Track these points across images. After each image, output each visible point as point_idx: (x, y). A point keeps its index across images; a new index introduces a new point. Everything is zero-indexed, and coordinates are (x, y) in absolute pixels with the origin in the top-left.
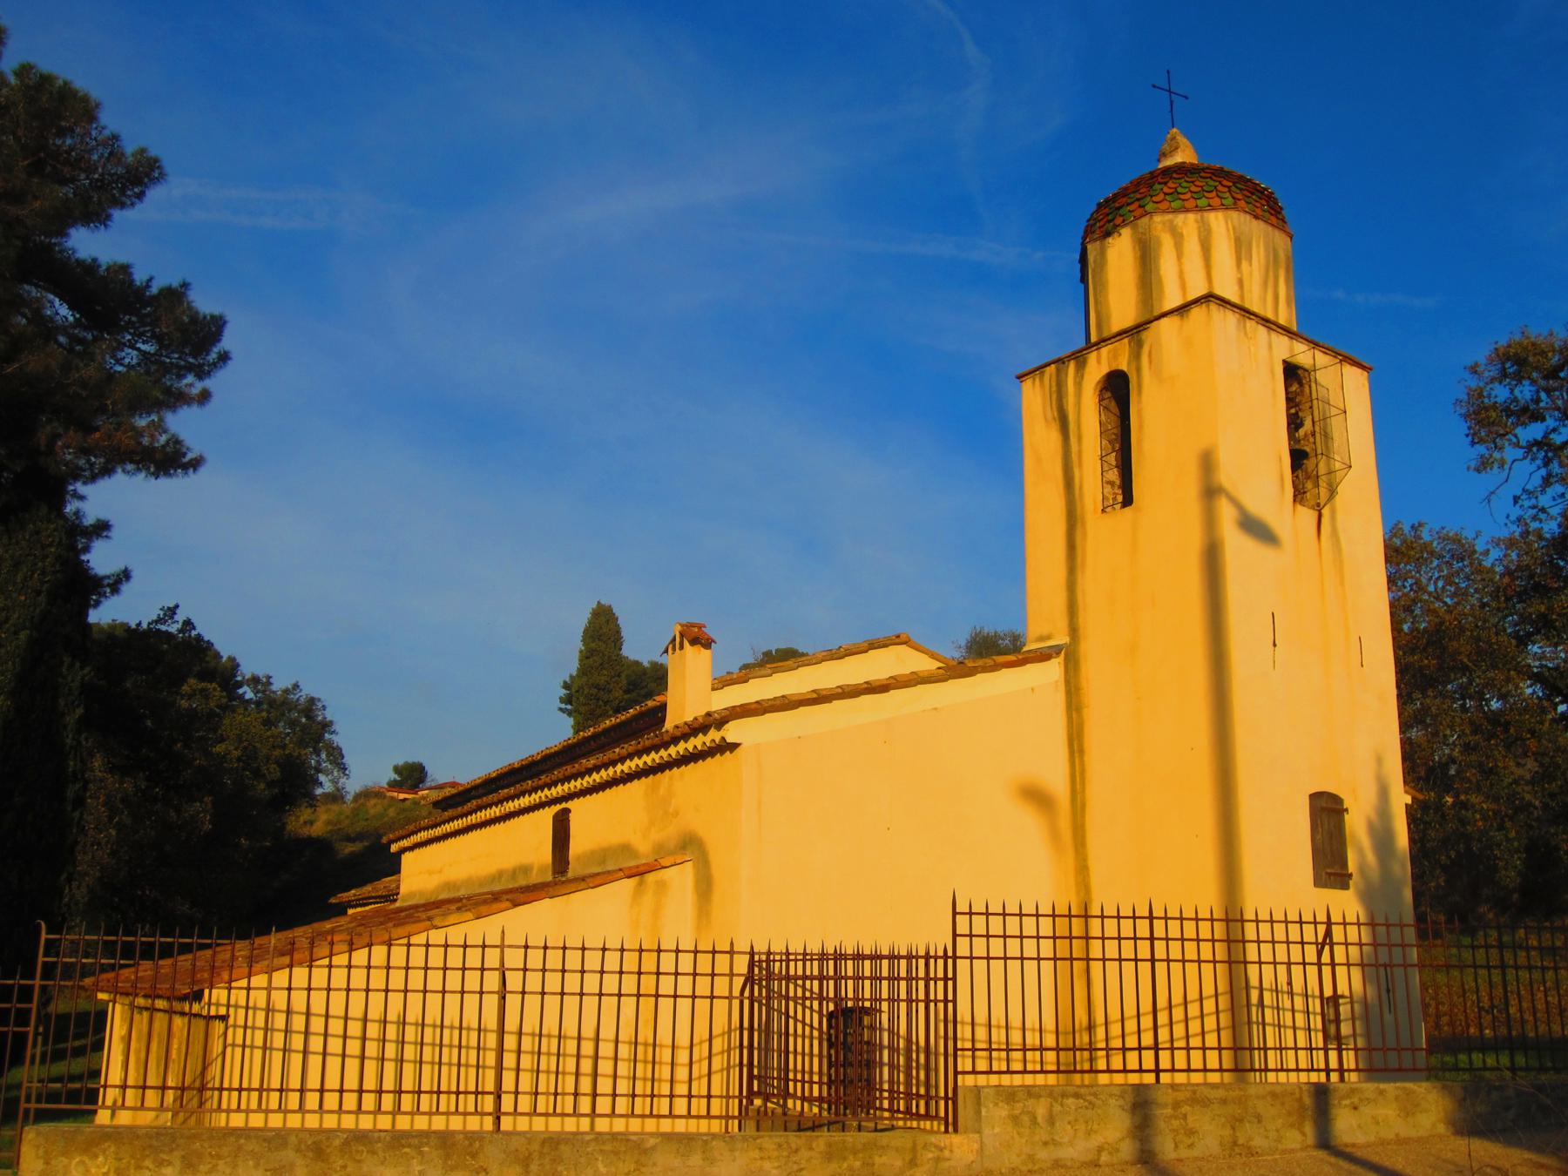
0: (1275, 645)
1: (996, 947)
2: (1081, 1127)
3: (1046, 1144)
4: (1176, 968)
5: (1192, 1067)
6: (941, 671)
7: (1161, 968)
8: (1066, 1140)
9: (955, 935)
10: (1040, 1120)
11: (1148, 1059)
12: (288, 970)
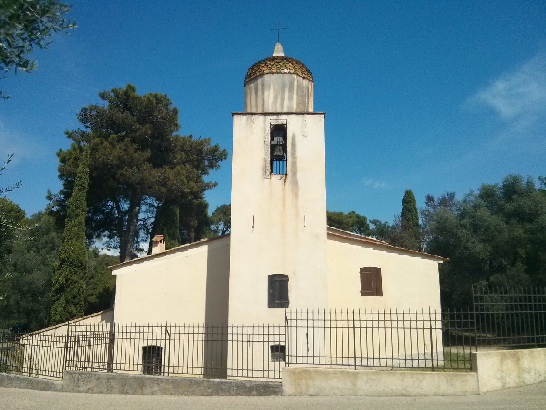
0: (253, 227)
1: (316, 324)
2: (85, 382)
3: (76, 386)
4: (177, 342)
5: (388, 366)
6: (164, 243)
7: (33, 347)
8: (81, 386)
9: (68, 331)
10: (76, 380)
11: (352, 362)
12: (67, 326)
